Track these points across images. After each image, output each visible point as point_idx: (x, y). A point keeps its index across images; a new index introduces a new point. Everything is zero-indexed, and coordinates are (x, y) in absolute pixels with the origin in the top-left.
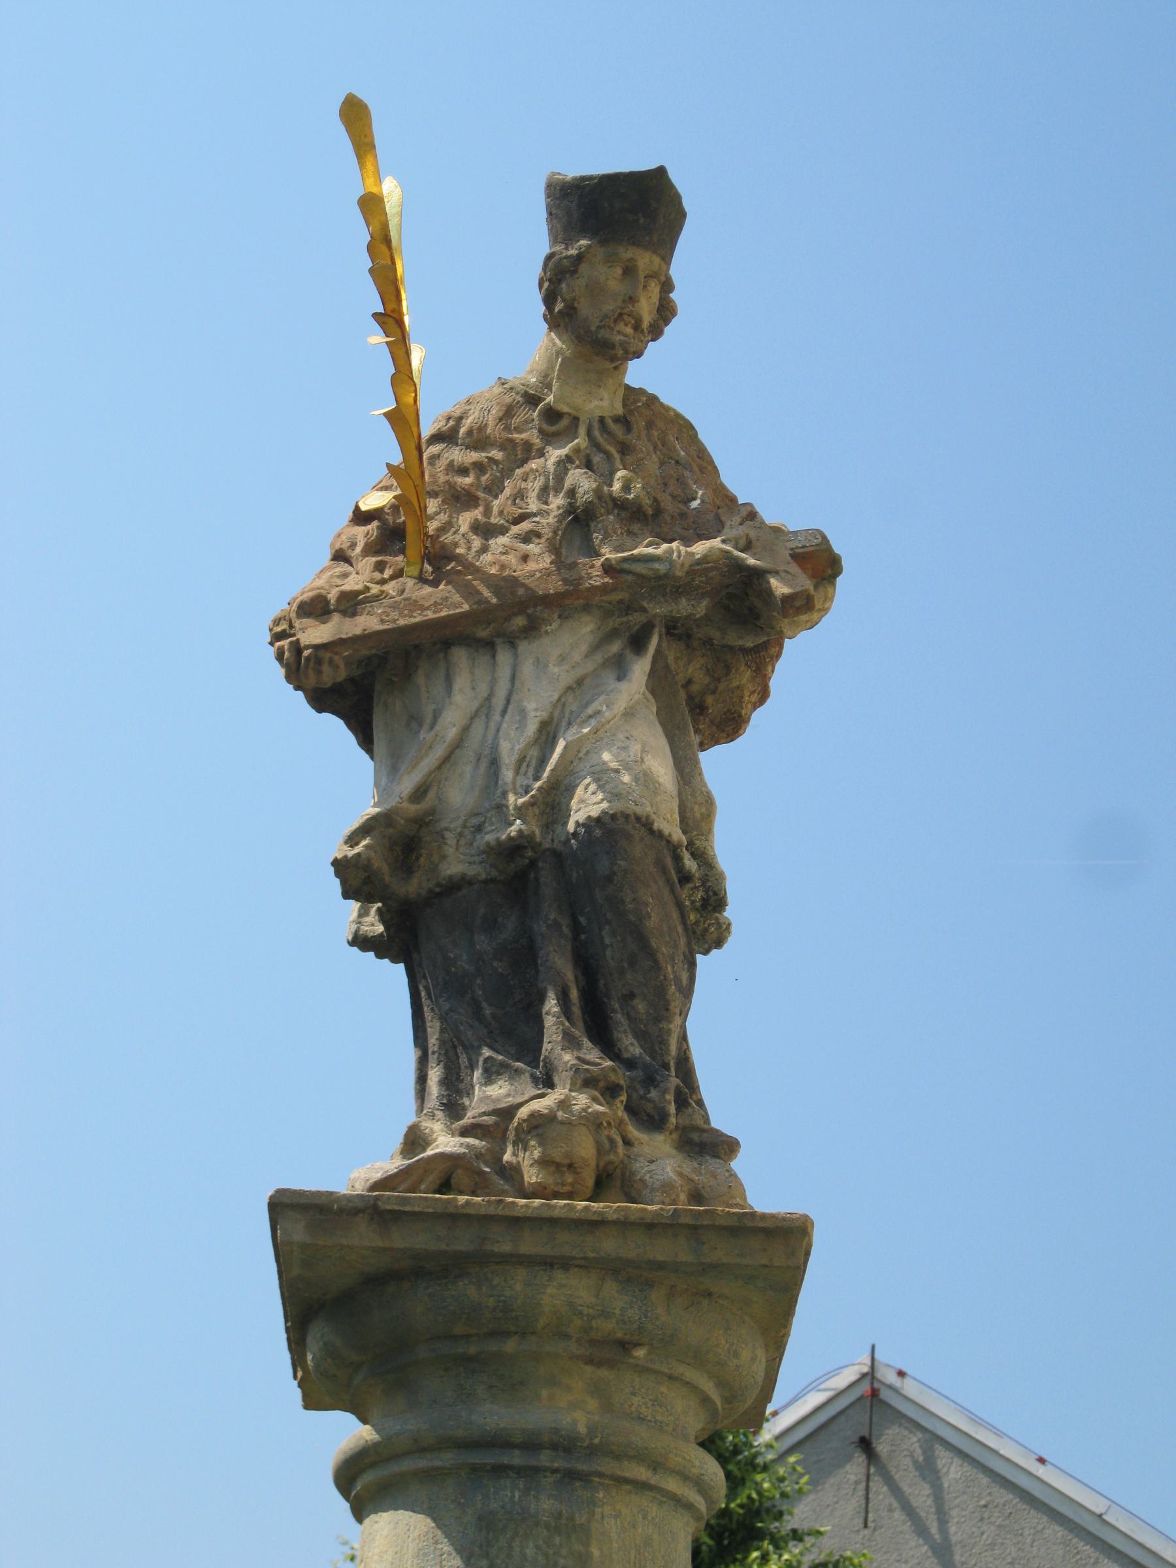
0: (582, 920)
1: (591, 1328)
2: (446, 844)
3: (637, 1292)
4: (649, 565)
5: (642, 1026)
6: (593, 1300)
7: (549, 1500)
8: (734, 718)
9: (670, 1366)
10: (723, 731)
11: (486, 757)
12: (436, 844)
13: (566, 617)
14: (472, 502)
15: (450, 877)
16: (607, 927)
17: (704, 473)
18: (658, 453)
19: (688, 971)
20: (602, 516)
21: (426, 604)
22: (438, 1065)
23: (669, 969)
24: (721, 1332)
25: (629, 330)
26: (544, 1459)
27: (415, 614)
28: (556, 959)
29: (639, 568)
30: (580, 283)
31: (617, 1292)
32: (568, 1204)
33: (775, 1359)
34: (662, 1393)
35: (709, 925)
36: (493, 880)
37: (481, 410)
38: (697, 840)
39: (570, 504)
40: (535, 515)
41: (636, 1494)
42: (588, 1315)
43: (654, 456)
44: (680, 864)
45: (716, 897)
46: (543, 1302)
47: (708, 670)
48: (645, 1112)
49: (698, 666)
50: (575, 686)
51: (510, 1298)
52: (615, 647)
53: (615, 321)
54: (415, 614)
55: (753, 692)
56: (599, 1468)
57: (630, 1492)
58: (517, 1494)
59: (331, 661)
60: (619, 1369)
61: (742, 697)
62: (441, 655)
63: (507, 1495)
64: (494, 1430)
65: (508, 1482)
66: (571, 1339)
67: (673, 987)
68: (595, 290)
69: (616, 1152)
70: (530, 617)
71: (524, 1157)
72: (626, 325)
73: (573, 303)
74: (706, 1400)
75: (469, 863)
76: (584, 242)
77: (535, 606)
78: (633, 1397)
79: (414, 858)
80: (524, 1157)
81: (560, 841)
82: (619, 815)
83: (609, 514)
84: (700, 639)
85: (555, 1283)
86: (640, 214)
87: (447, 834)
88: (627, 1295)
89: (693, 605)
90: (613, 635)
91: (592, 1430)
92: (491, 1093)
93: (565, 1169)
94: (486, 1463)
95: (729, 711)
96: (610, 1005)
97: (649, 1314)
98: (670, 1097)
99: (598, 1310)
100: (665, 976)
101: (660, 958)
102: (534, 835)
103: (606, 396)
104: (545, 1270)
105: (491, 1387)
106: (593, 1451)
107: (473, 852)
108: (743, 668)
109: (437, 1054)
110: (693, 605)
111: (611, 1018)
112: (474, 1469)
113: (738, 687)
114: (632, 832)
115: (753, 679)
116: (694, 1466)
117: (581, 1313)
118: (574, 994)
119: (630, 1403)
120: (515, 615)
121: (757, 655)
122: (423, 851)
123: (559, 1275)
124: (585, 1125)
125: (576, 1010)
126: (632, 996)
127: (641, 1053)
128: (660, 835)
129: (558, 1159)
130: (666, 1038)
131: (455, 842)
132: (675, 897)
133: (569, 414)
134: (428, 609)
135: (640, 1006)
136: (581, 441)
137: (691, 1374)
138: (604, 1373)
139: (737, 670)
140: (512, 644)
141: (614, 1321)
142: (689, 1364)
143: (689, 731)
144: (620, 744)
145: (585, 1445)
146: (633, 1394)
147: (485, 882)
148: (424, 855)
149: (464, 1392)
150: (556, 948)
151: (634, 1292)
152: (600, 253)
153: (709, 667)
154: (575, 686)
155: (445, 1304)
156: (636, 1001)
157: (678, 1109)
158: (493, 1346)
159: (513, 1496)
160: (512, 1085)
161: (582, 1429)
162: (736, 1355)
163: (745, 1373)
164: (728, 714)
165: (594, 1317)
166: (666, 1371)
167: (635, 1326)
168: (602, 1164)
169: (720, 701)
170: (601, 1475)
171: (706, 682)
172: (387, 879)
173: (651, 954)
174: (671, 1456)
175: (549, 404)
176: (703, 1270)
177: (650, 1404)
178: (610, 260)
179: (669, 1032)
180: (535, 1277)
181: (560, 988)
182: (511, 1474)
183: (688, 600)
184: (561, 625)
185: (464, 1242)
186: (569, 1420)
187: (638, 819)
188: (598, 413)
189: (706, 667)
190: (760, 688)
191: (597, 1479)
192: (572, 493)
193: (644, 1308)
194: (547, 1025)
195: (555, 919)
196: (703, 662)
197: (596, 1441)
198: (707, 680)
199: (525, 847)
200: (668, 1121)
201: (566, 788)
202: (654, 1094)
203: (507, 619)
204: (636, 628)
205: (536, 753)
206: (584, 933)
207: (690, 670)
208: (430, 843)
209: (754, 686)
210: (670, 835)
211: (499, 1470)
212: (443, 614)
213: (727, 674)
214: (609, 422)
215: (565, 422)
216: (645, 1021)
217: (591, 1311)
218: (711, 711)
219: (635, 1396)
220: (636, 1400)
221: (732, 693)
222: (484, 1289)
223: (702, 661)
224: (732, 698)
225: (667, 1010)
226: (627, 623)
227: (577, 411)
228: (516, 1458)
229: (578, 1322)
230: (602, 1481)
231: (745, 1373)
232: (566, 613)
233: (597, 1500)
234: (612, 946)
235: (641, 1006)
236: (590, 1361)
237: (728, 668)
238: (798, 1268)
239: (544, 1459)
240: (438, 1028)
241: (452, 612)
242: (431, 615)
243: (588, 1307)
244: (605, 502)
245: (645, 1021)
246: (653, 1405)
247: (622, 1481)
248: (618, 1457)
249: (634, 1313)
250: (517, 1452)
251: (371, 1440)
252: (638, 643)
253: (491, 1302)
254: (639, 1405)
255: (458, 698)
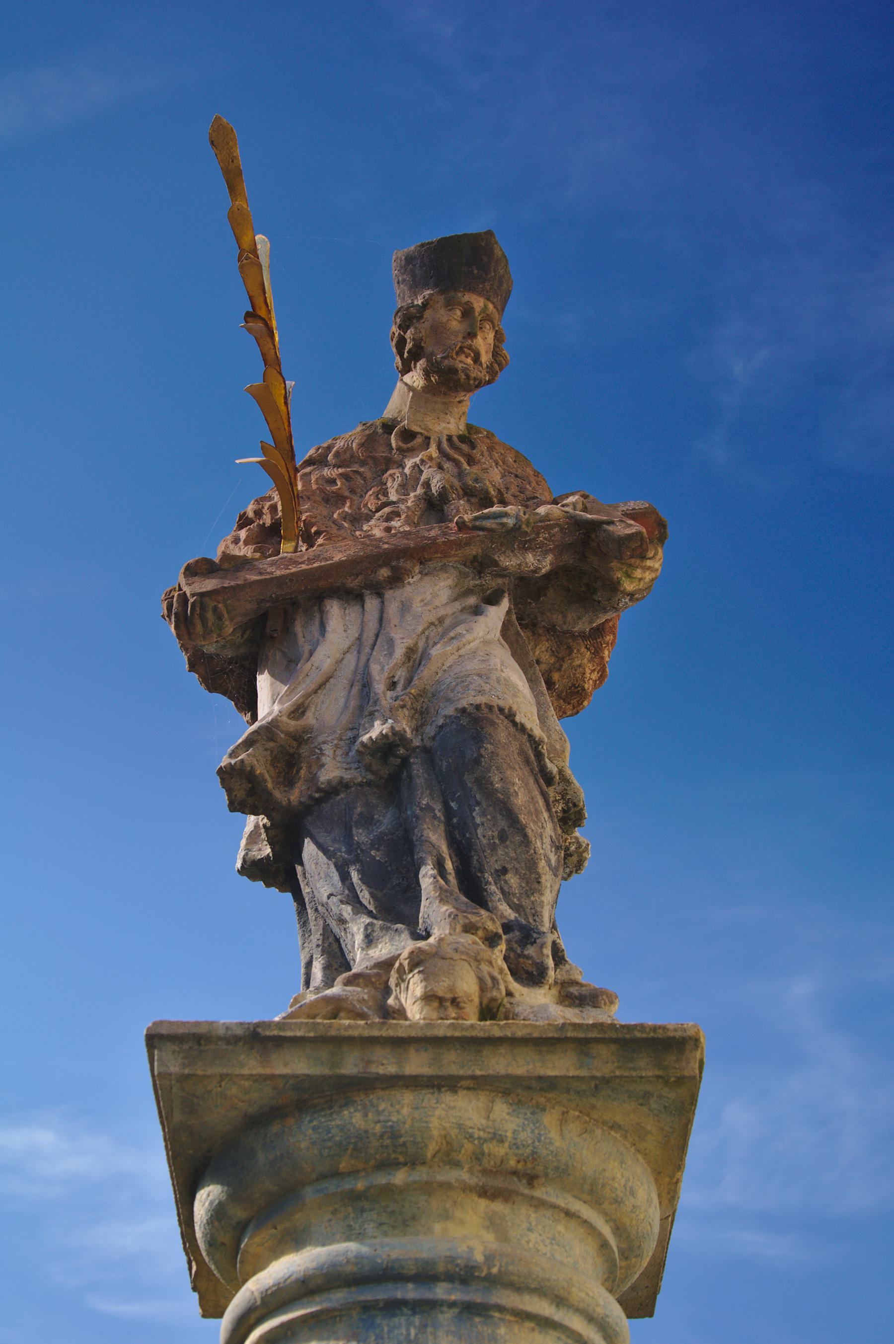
0: (453, 804)
1: (483, 1154)
2: (323, 754)
3: (529, 1115)
4: (498, 521)
5: (515, 900)
6: (484, 1122)
7: (447, 1336)
8: (579, 691)
9: (567, 1201)
10: (569, 704)
11: (358, 682)
12: (314, 757)
13: (426, 574)
14: (340, 502)
15: (329, 782)
16: (477, 808)
17: (539, 485)
18: (499, 468)
19: (556, 854)
20: (454, 500)
21: (300, 560)
22: (322, 955)
23: (539, 844)
24: (616, 1164)
25: (469, 361)
26: (441, 1291)
27: (290, 567)
28: (431, 835)
29: (488, 524)
30: (424, 326)
31: (508, 1114)
32: (453, 1023)
33: (667, 1217)
34: (560, 1232)
35: (570, 843)
36: (369, 784)
37: (345, 442)
38: (555, 760)
39: (425, 493)
40: (394, 503)
41: (540, 1332)
42: (479, 1138)
43: (496, 469)
44: (542, 762)
45: (576, 809)
46: (431, 1125)
47: (553, 651)
48: (524, 970)
49: (543, 649)
50: (436, 623)
51: (397, 1122)
52: (472, 600)
53: (457, 353)
54: (290, 567)
55: (593, 671)
56: (499, 1301)
57: (533, 1330)
58: (413, 1332)
59: (215, 609)
60: (514, 1203)
61: (584, 674)
62: (316, 608)
63: (402, 1334)
64: (385, 1262)
65: (403, 1319)
66: (463, 1169)
67: (543, 861)
68: (437, 330)
69: (498, 989)
70: (395, 569)
71: (406, 998)
72: (467, 357)
73: (420, 343)
74: (604, 1245)
75: (346, 769)
76: (427, 292)
77: (398, 559)
78: (530, 1233)
79: (294, 772)
80: (406, 998)
81: (429, 738)
82: (483, 706)
83: (459, 499)
84: (544, 627)
85: (443, 1106)
86: (474, 267)
87: (324, 747)
88: (518, 1117)
89: (538, 560)
90: (468, 592)
91: (489, 1258)
92: (373, 955)
93: (448, 1004)
94: (378, 1300)
95: (574, 685)
96: (484, 878)
97: (543, 1138)
98: (548, 951)
99: (489, 1133)
100: (534, 850)
101: (529, 833)
102: (405, 732)
103: (452, 420)
104: (433, 1093)
105: (381, 1224)
106: (493, 1281)
107: (349, 760)
108: (583, 650)
109: (321, 947)
110: (538, 560)
111: (486, 890)
112: (367, 1307)
113: (580, 666)
114: (497, 721)
115: (591, 660)
116: (598, 1305)
117: (471, 1136)
118: (449, 866)
119: (526, 1239)
120: (380, 566)
121: (595, 641)
122: (303, 764)
123: (448, 1098)
124: (466, 960)
125: (452, 878)
126: (504, 871)
127: (516, 917)
128: (522, 729)
129: (441, 993)
130: (538, 910)
131: (332, 752)
132: (539, 786)
133: (421, 434)
134: (303, 563)
135: (512, 881)
136: (433, 450)
137: (587, 1212)
138: (498, 1206)
139: (578, 650)
140: (380, 595)
141: (506, 1145)
142: (585, 1202)
143: (540, 682)
144: (480, 658)
145: (483, 1275)
146: (529, 1230)
147: (361, 785)
148: (304, 768)
149: (353, 1232)
150: (430, 827)
151: (526, 1114)
152: (441, 299)
153: (553, 649)
154: (436, 623)
155: (330, 1135)
156: (508, 876)
157: (557, 965)
158: (381, 1179)
159: (409, 1334)
160: (393, 945)
161: (479, 1257)
162: (633, 1193)
163: (642, 1217)
164: (573, 688)
165: (485, 1141)
166: (563, 1205)
167: (528, 1151)
168: (485, 1001)
169: (565, 677)
170: (501, 1309)
171: (552, 662)
172: (270, 785)
173: (521, 830)
174: (574, 1290)
175: (404, 426)
176: (596, 1087)
177: (548, 1241)
178: (450, 304)
179: (542, 904)
180: (423, 1100)
181: (435, 859)
182: (405, 1310)
183: (534, 556)
184: (421, 579)
185: (350, 1066)
186: (464, 1248)
187: (501, 710)
188: (446, 432)
189: (551, 649)
190: (599, 668)
191: (497, 1315)
192: (427, 485)
193: (536, 1131)
194: (423, 886)
195: (427, 804)
196: (548, 645)
197: (495, 1270)
198: (552, 660)
199: (398, 746)
200: (547, 974)
201: (433, 694)
202: (530, 951)
203: (374, 571)
204: (489, 592)
205: (403, 674)
206: (456, 817)
207: (537, 653)
208: (309, 757)
209: (594, 666)
210: (531, 730)
211: (393, 1307)
212: (315, 565)
213: (570, 654)
214: (455, 439)
215: (419, 440)
216: (518, 895)
217: (482, 1134)
218: (557, 686)
219: (533, 1232)
220: (533, 1236)
221: (576, 670)
222: (370, 1115)
223: (547, 644)
224: (575, 674)
225: (539, 882)
226: (480, 586)
227: (427, 431)
228: (410, 1292)
229: (468, 1147)
230: (502, 1316)
231: (642, 1217)
232: (426, 571)
233: (499, 1337)
234: (483, 824)
235: (513, 880)
236: (484, 1193)
237: (570, 650)
238: (695, 1077)
239: (441, 1291)
240: (322, 926)
241: (323, 564)
242: (304, 567)
243: (479, 1129)
244: (456, 489)
245: (518, 895)
246: (551, 1243)
247: (524, 1316)
248: (518, 1288)
249: (525, 1136)
250: (410, 1286)
251: (257, 1290)
252: (493, 600)
253: (378, 1128)
254: (536, 1242)
255: (330, 636)
